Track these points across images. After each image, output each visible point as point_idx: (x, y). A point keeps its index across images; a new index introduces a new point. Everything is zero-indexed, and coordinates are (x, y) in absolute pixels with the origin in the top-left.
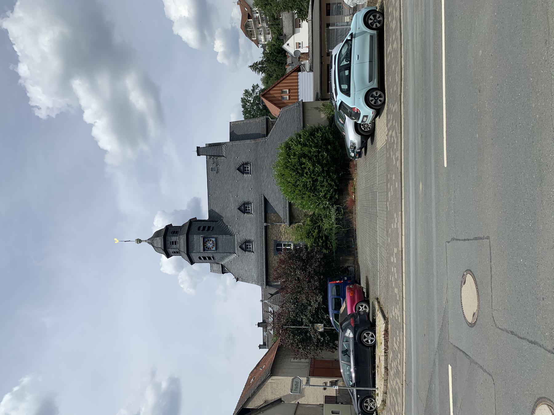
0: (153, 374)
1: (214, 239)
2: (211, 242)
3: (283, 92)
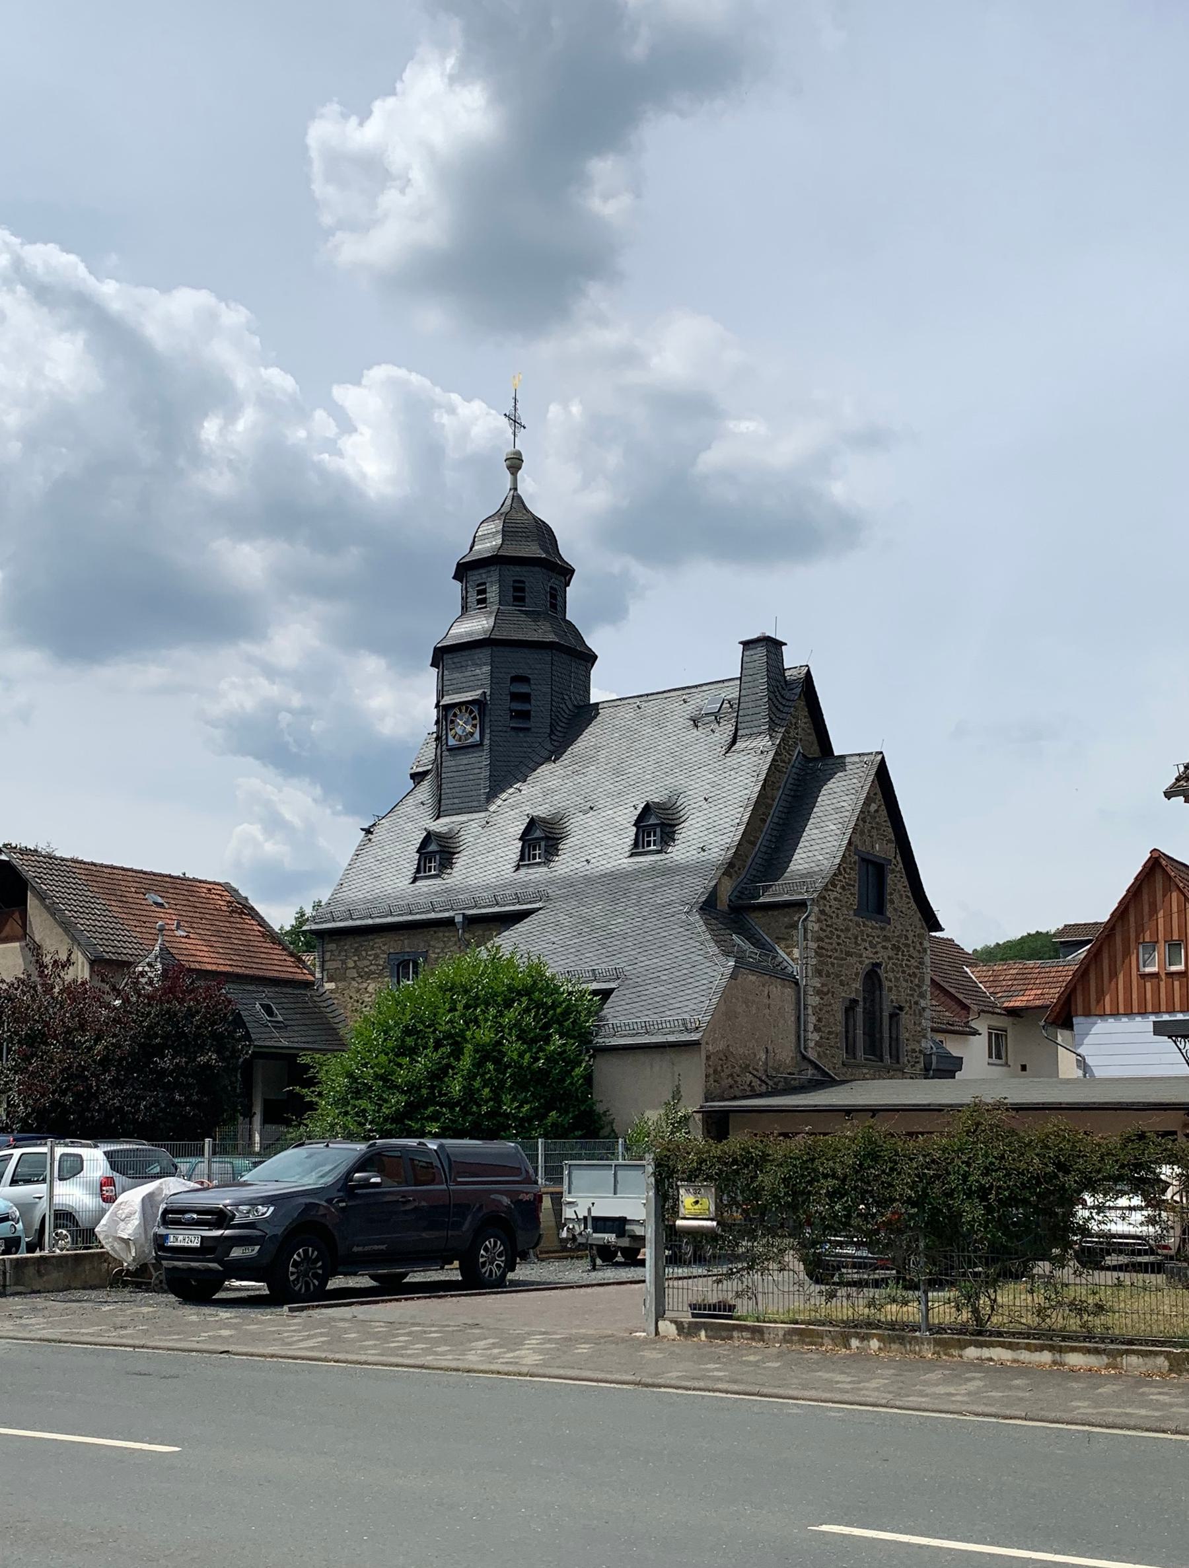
0: (873, 439)
1: (477, 736)
2: (469, 728)
3: (1174, 946)
